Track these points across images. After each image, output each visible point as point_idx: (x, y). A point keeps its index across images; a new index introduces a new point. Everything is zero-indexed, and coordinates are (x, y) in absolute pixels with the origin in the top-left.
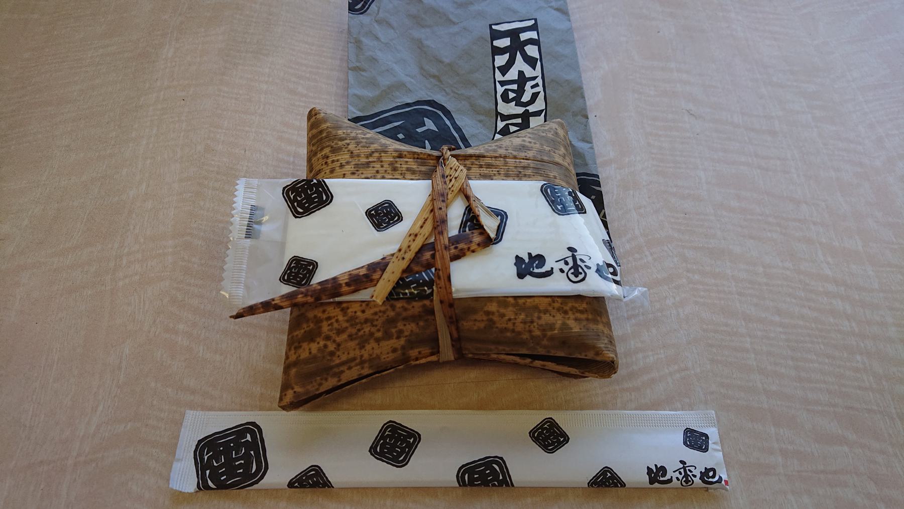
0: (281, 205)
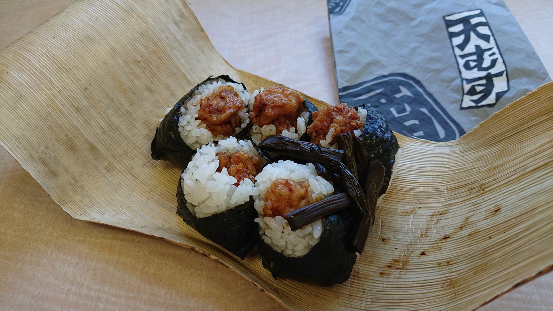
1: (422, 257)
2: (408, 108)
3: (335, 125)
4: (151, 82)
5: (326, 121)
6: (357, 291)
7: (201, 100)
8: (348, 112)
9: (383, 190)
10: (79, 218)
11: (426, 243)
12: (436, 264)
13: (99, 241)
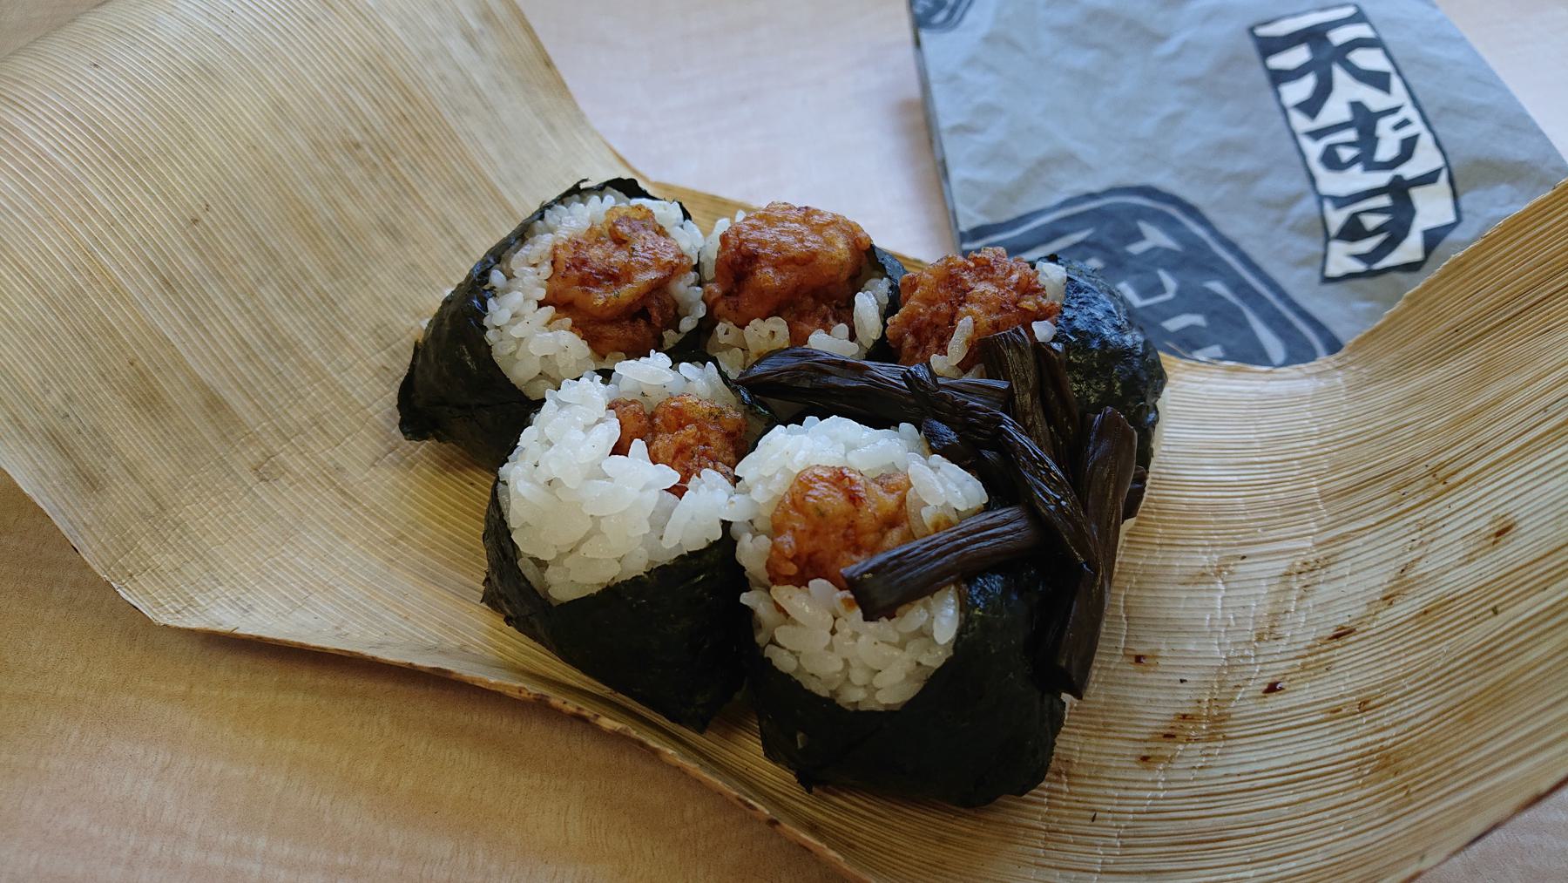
1: (1272, 697)
2: (1170, 283)
3: (975, 309)
4: (395, 207)
6: (1069, 816)
7: (556, 247)
8: (1011, 272)
9: (1131, 510)
10: (170, 623)
11: (1277, 658)
12: (1323, 711)
13: (234, 695)
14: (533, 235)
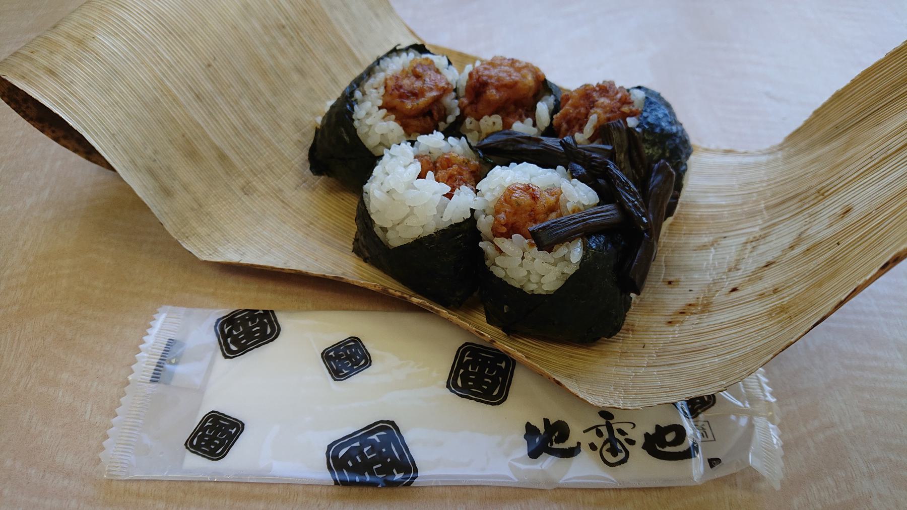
0: (211, 339)
5: (582, 106)
7: (386, 79)
9: (670, 212)
13: (237, 293)
14: (374, 73)
